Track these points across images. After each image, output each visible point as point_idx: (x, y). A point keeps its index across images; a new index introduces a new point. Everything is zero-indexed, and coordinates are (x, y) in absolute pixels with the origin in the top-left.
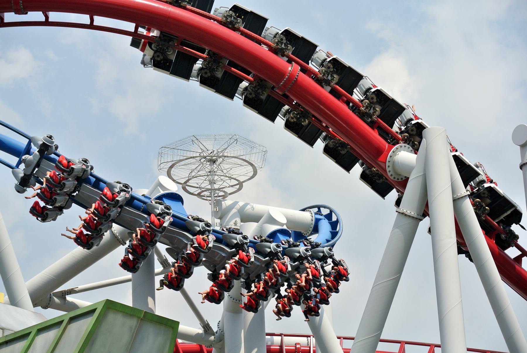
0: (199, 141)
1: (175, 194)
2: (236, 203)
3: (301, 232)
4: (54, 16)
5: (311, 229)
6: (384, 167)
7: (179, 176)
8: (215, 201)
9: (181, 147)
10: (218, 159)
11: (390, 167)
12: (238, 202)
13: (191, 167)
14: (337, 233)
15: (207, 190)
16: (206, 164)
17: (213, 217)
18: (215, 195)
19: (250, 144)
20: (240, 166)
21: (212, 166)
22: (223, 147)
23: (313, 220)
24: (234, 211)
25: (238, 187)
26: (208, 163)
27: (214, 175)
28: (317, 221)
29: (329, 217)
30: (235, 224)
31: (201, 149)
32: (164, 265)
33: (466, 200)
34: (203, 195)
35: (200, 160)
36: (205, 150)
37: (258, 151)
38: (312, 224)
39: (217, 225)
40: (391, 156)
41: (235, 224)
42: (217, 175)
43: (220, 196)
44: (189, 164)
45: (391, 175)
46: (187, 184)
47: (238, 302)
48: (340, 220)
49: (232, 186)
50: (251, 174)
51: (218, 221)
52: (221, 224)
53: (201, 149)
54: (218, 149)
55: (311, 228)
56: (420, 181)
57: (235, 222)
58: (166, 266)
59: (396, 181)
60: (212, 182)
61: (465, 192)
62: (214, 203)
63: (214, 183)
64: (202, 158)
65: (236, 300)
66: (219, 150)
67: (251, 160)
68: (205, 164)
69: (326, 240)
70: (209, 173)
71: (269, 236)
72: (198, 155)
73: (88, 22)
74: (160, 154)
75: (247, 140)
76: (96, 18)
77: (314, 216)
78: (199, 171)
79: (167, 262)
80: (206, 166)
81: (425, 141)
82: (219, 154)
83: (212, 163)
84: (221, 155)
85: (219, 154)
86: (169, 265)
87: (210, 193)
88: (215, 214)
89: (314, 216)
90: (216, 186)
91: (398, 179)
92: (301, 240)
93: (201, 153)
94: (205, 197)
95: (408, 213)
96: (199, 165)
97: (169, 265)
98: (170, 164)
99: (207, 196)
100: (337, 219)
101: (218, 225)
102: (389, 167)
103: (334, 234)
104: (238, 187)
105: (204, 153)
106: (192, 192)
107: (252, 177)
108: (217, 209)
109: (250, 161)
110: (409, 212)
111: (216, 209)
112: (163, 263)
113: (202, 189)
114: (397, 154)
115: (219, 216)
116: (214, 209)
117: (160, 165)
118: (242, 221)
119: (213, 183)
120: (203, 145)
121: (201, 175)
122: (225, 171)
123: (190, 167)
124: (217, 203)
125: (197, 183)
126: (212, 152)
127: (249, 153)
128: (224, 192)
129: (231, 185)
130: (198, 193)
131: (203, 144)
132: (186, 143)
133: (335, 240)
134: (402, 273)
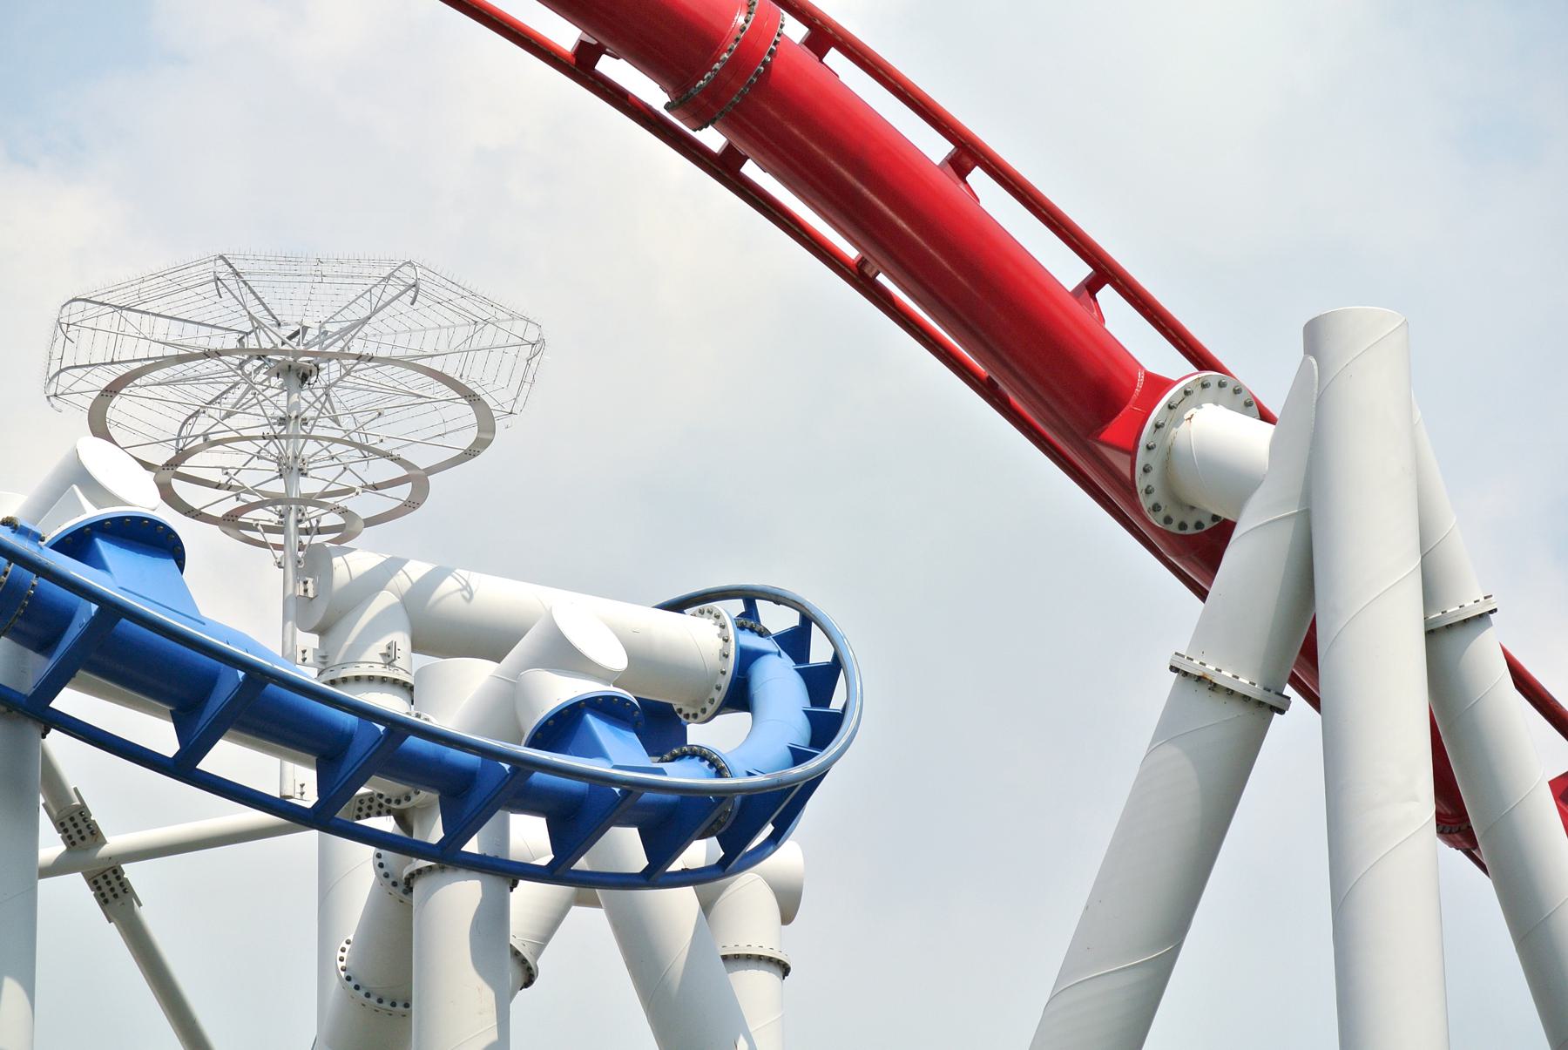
0: (244, 282)
1: (604, 697)
2: (393, 566)
3: (671, 705)
5: (719, 696)
6: (1127, 473)
7: (135, 432)
8: (300, 554)
9: (160, 302)
10: (321, 365)
11: (1150, 474)
12: (405, 561)
13: (195, 391)
14: (837, 720)
15: (273, 500)
16: (267, 383)
17: (290, 624)
18: (301, 526)
19: (469, 307)
21: (296, 395)
22: (351, 315)
23: (726, 656)
24: (385, 600)
25: (404, 491)
26: (275, 381)
27: (303, 437)
28: (748, 658)
29: (795, 643)
30: (389, 658)
31: (252, 318)
32: (73, 831)
33: (1480, 637)
34: (251, 521)
35: (241, 366)
36: (267, 321)
37: (501, 339)
38: (724, 673)
39: (304, 660)
40: (1158, 426)
41: (389, 658)
42: (316, 439)
43: (319, 531)
44: (188, 379)
45: (1156, 508)
46: (179, 469)
47: (390, 1007)
48: (848, 656)
49: (375, 487)
51: (310, 641)
52: (324, 657)
53: (252, 318)
54: (327, 322)
55: (719, 688)
56: (1283, 540)
57: (389, 648)
58: (79, 836)
59: (1174, 534)
60: (291, 468)
61: (1478, 601)
62: (299, 562)
63: (300, 470)
64: (250, 358)
65: (380, 1001)
66: (328, 327)
67: (465, 375)
68: (261, 384)
69: (788, 752)
70: (280, 424)
71: (551, 722)
72: (231, 342)
74: (64, 327)
75: (460, 291)
77: (732, 638)
78: (229, 415)
79: (84, 820)
80: (269, 393)
81: (1316, 367)
82: (327, 342)
83: (295, 381)
84: (335, 349)
85: (327, 342)
86: (92, 833)
87: (281, 516)
88: (300, 611)
89: (732, 638)
90: (307, 486)
91: (1183, 526)
92: (676, 751)
93: (247, 334)
94: (258, 531)
95: (1225, 677)
96: (230, 385)
97: (92, 833)
98: (104, 378)
99: (268, 529)
100: (836, 658)
101: (310, 660)
102: (1146, 470)
103: (824, 727)
104: (404, 491)
105: (262, 335)
106: (197, 507)
107: (470, 453)
108: (310, 586)
109: (461, 381)
110: (1230, 676)
111: (302, 587)
112: (69, 825)
113: (243, 496)
114: (1187, 415)
115: (317, 620)
116: (295, 588)
117: (58, 374)
118: (417, 647)
119: (295, 469)
120: (258, 298)
121: (245, 433)
122: (347, 422)
123: (189, 394)
124: (312, 564)
125: (223, 468)
126: (297, 333)
127: (461, 348)
128: (344, 512)
129: (370, 483)
130: (227, 515)
131: (259, 294)
132: (186, 285)
133: (829, 755)
134: (1184, 938)
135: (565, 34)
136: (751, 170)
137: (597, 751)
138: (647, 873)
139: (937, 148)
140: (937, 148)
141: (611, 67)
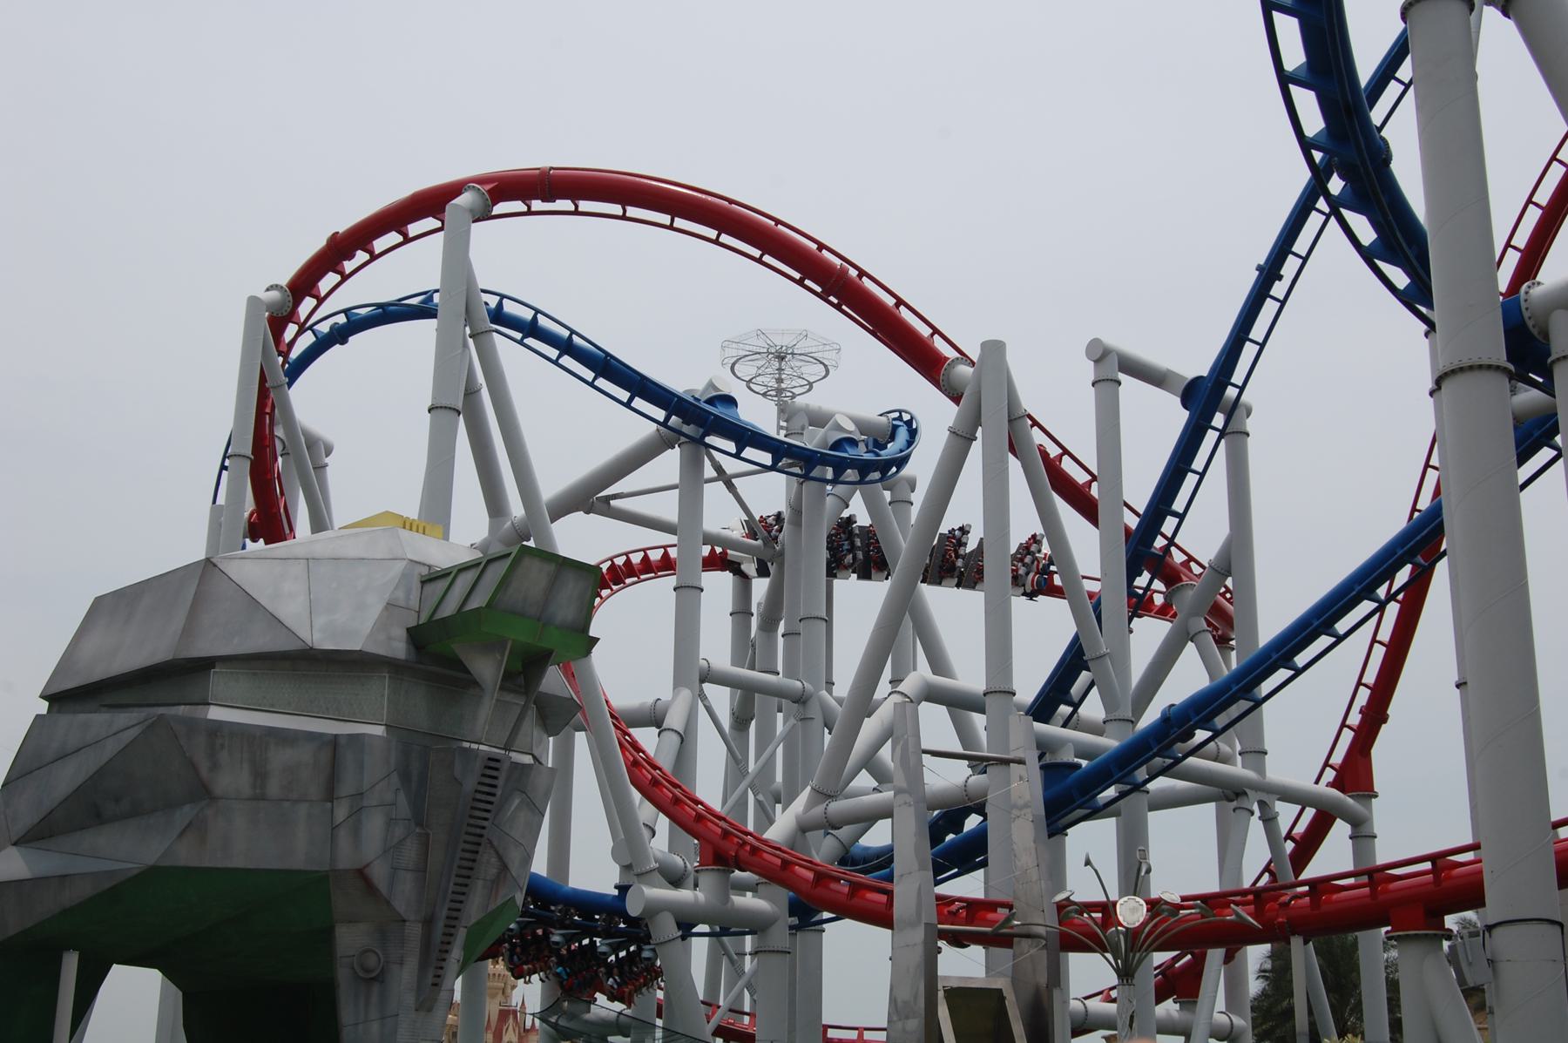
4: (725, 238)
50: (824, 374)
60: (780, 381)
90: (783, 386)
107: (824, 377)
128: (791, 392)
135: (797, 276)
136: (844, 307)
137: (846, 451)
138: (860, 481)
140: (814, 246)
141: (807, 282)
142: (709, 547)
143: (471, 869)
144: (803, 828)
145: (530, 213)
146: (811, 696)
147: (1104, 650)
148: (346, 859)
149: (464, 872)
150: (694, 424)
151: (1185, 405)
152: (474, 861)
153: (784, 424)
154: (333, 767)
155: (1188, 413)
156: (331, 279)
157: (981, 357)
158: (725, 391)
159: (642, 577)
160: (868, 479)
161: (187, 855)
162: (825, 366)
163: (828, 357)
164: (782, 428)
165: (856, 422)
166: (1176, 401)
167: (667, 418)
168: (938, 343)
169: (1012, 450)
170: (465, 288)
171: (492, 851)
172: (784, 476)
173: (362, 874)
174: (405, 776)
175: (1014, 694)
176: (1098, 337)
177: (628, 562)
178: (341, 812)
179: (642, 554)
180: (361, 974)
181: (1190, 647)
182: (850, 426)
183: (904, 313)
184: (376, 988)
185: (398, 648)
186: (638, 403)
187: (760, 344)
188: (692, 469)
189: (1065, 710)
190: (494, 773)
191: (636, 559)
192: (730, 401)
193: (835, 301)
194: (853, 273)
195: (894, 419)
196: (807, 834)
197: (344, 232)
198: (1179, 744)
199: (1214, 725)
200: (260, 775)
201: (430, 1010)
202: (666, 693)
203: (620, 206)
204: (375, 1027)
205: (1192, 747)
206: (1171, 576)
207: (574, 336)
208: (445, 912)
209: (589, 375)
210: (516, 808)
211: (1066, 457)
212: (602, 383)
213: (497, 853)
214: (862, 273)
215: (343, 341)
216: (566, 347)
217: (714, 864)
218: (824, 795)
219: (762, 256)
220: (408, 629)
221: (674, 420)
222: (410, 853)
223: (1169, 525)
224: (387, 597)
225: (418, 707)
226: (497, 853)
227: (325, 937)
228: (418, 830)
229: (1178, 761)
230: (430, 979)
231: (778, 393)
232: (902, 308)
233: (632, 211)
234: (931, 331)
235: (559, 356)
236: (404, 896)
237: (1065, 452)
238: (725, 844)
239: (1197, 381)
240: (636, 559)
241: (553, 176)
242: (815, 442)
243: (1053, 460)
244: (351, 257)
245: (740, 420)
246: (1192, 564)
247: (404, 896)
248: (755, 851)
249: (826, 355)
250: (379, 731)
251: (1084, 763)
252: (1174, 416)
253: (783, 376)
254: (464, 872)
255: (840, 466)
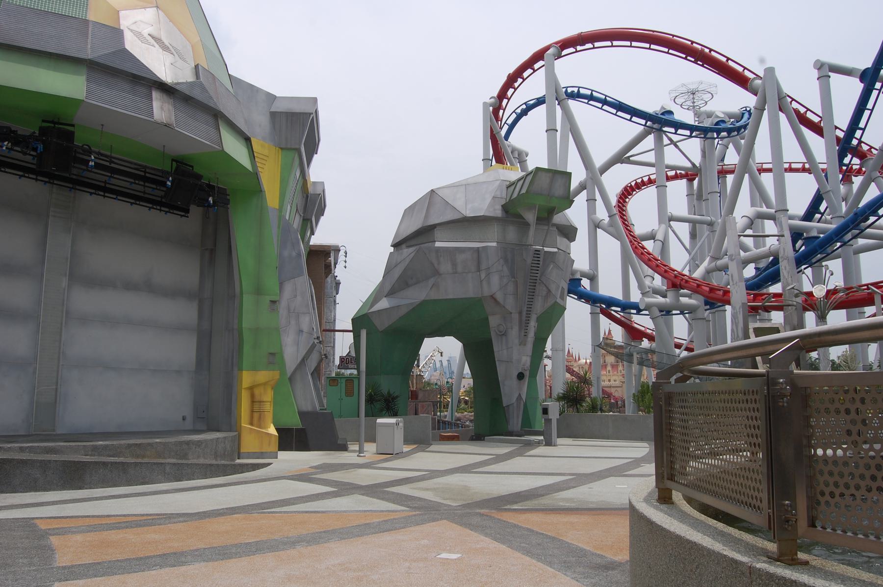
4: (671, 51)
15: (691, 106)
20: (522, 181)
50: (711, 97)
60: (694, 102)
73: (611, 45)
76: (633, 43)
90: (695, 104)
98: (674, 98)
104: (704, 104)
107: (712, 98)
136: (705, 65)
137: (721, 126)
139: (689, 43)
140: (690, 43)
141: (689, 58)
142: (675, 171)
143: (534, 292)
144: (708, 272)
145: (577, 51)
146: (715, 222)
147: (829, 189)
148: (486, 292)
149: (531, 294)
150: (657, 123)
151: (861, 81)
152: (535, 289)
153: (697, 119)
154: (479, 259)
155: (863, 85)
156: (511, 91)
157: (764, 75)
158: (668, 109)
159: (649, 186)
160: (731, 135)
161: (434, 296)
162: (712, 94)
163: (712, 90)
164: (696, 121)
165: (724, 113)
166: (858, 80)
167: (646, 123)
168: (747, 73)
169: (781, 110)
170: (554, 84)
171: (543, 285)
172: (699, 139)
173: (492, 297)
174: (506, 260)
175: (788, 211)
176: (818, 59)
177: (642, 181)
178: (483, 276)
179: (648, 177)
180: (498, 333)
181: (873, 184)
182: (722, 115)
183: (731, 63)
184: (504, 338)
185: (499, 213)
186: (634, 119)
187: (684, 89)
188: (659, 141)
189: (818, 216)
190: (538, 256)
191: (646, 179)
192: (670, 113)
193: (701, 63)
194: (707, 51)
195: (743, 111)
196: (710, 274)
197: (513, 72)
198: (863, 224)
199: (878, 213)
200: (454, 265)
201: (525, 345)
202: (656, 227)
203: (609, 42)
204: (505, 351)
205: (870, 223)
206: (862, 156)
207: (607, 98)
208: (525, 309)
209: (614, 111)
210: (552, 269)
211: (808, 112)
212: (619, 113)
213: (546, 286)
214: (711, 50)
215: (526, 114)
216: (605, 102)
217: (672, 288)
218: (715, 258)
219: (668, 51)
220: (502, 206)
221: (649, 123)
222: (511, 288)
223: (858, 134)
224: (493, 195)
225: (512, 234)
226: (546, 286)
227: (486, 320)
228: (513, 280)
229: (862, 231)
230: (523, 334)
231: (693, 108)
232: (729, 61)
233: (615, 43)
234: (743, 69)
235: (602, 106)
236: (510, 304)
237: (808, 110)
238: (675, 280)
239: (866, 71)
240: (646, 179)
241: (583, 35)
242: (708, 124)
243: (803, 114)
244: (516, 81)
245: (675, 119)
246: (872, 150)
247: (510, 304)
248: (687, 282)
249: (712, 89)
250: (494, 244)
251: (822, 236)
252: (856, 87)
253: (695, 101)
254: (531, 294)
255: (719, 132)
